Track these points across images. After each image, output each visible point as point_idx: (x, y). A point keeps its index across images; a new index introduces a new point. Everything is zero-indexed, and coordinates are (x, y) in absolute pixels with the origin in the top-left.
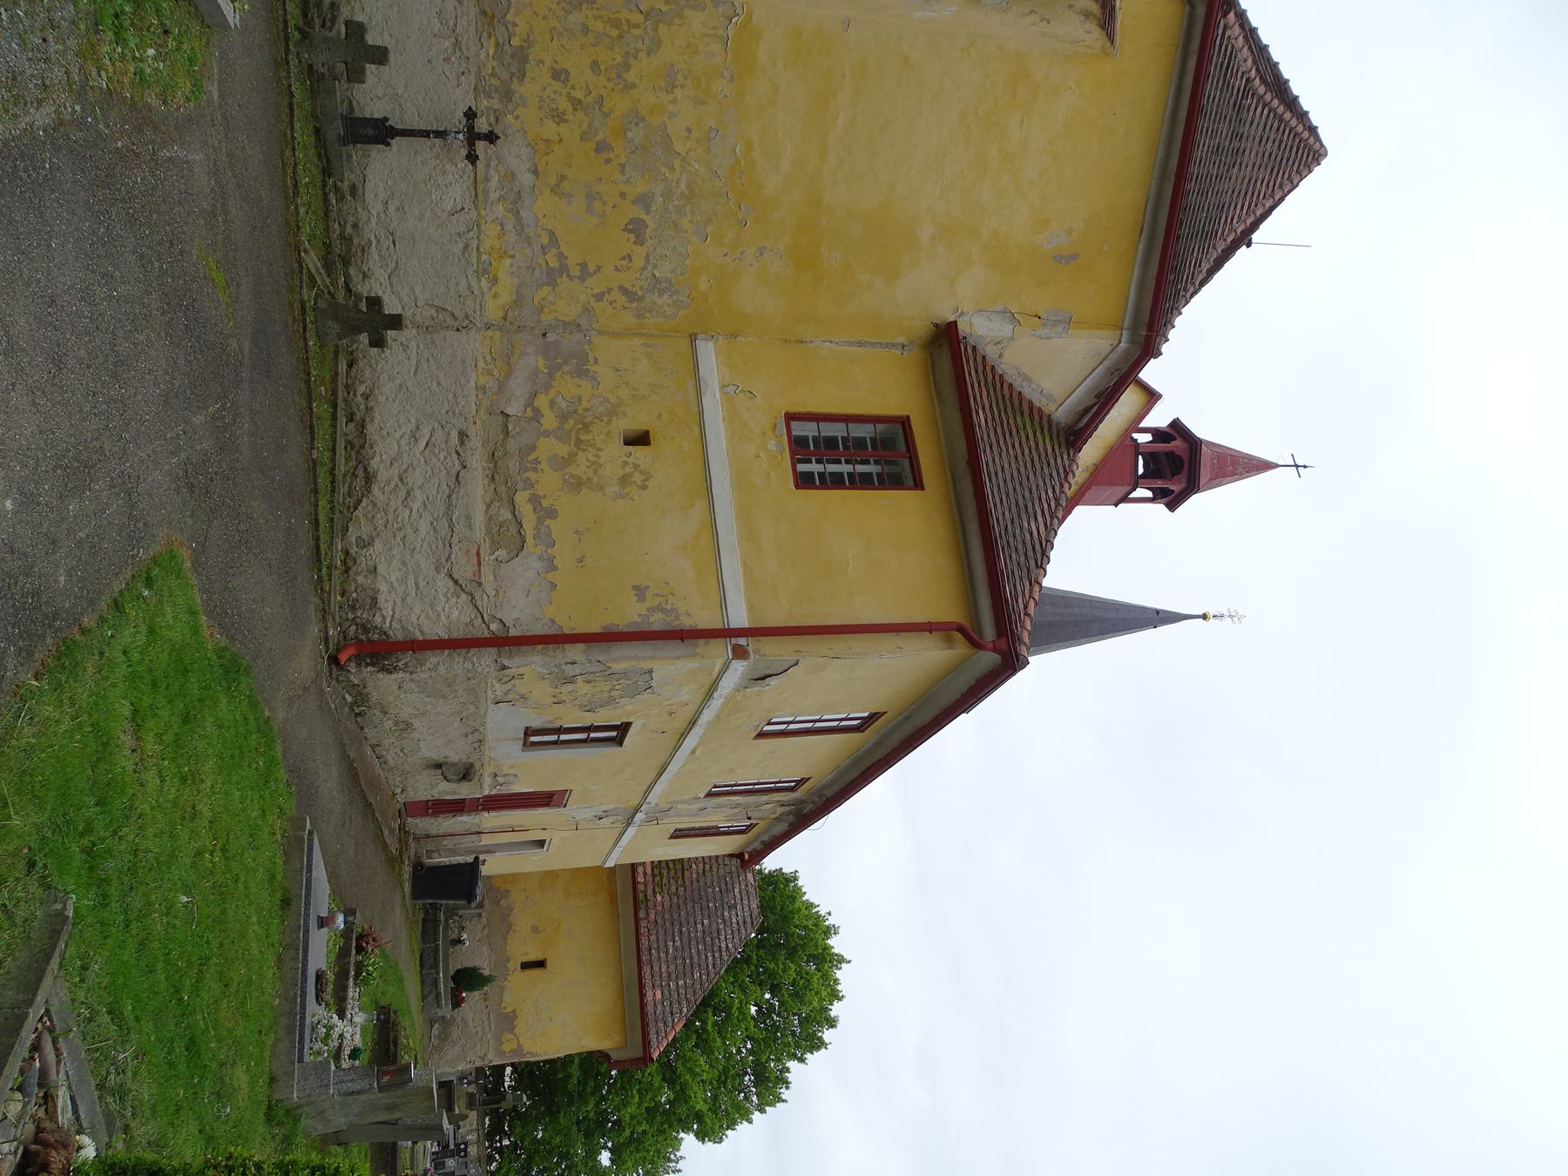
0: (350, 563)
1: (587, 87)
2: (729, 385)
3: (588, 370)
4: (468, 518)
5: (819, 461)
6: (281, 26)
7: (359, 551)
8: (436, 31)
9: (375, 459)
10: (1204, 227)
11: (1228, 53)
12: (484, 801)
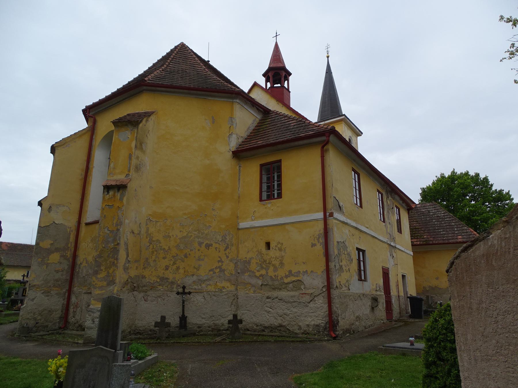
0: (306, 332)
1: (170, 260)
2: (252, 219)
3: (248, 260)
4: (292, 297)
5: (274, 191)
6: (157, 344)
7: (302, 330)
8: (156, 302)
9: (275, 324)
10: (204, 79)
11: (156, 78)
12: (386, 294)
